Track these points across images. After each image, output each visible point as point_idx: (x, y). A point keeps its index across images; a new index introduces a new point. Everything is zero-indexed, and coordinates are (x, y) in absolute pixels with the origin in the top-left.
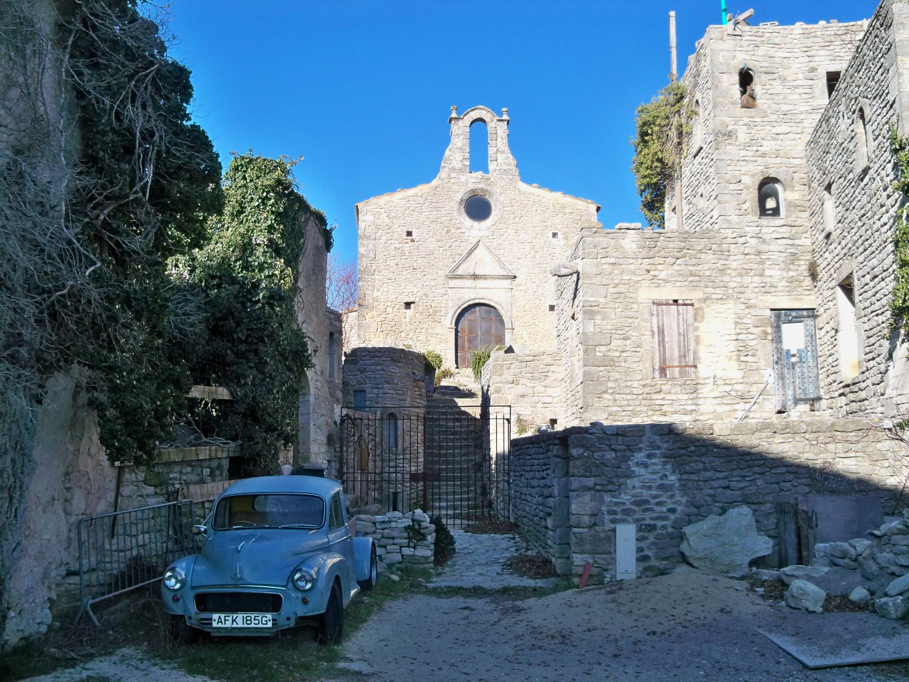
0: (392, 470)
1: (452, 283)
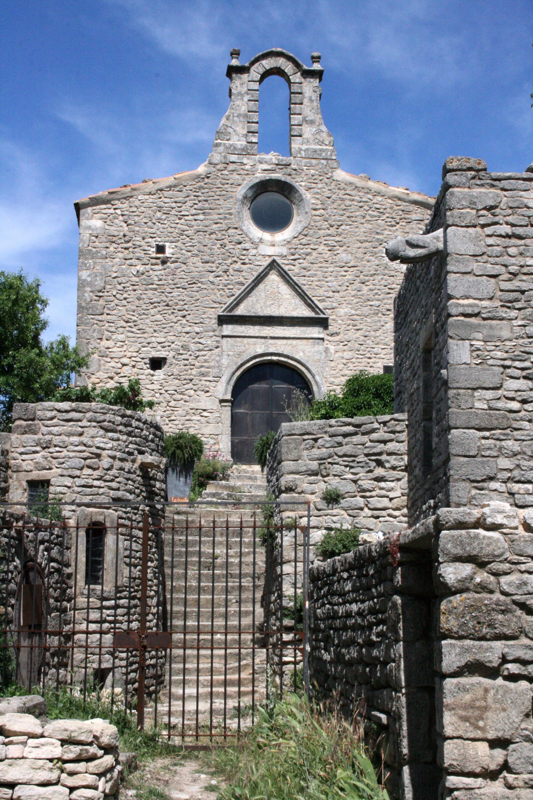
0: (93, 627)
1: (228, 329)
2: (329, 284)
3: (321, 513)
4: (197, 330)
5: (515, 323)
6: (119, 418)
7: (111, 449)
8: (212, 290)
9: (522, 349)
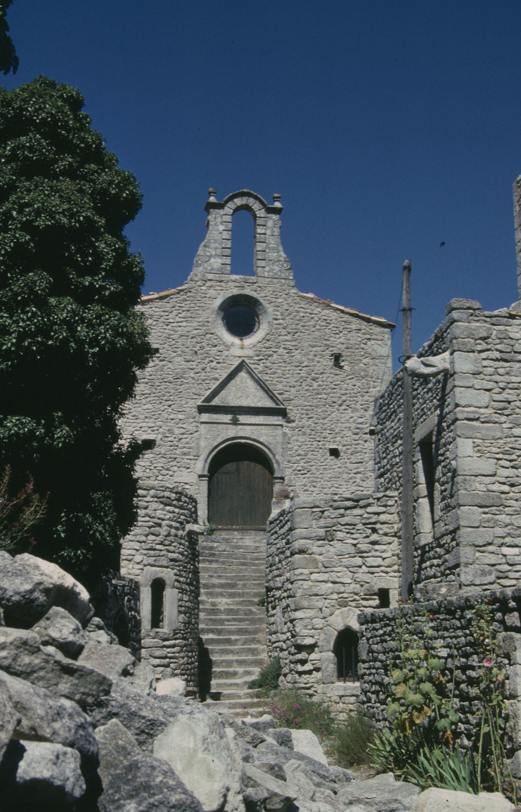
1: (205, 417)
2: (288, 380)
3: (328, 570)
4: (180, 417)
5: (504, 425)
6: (174, 495)
7: (169, 519)
8: (193, 384)
9: (510, 445)
